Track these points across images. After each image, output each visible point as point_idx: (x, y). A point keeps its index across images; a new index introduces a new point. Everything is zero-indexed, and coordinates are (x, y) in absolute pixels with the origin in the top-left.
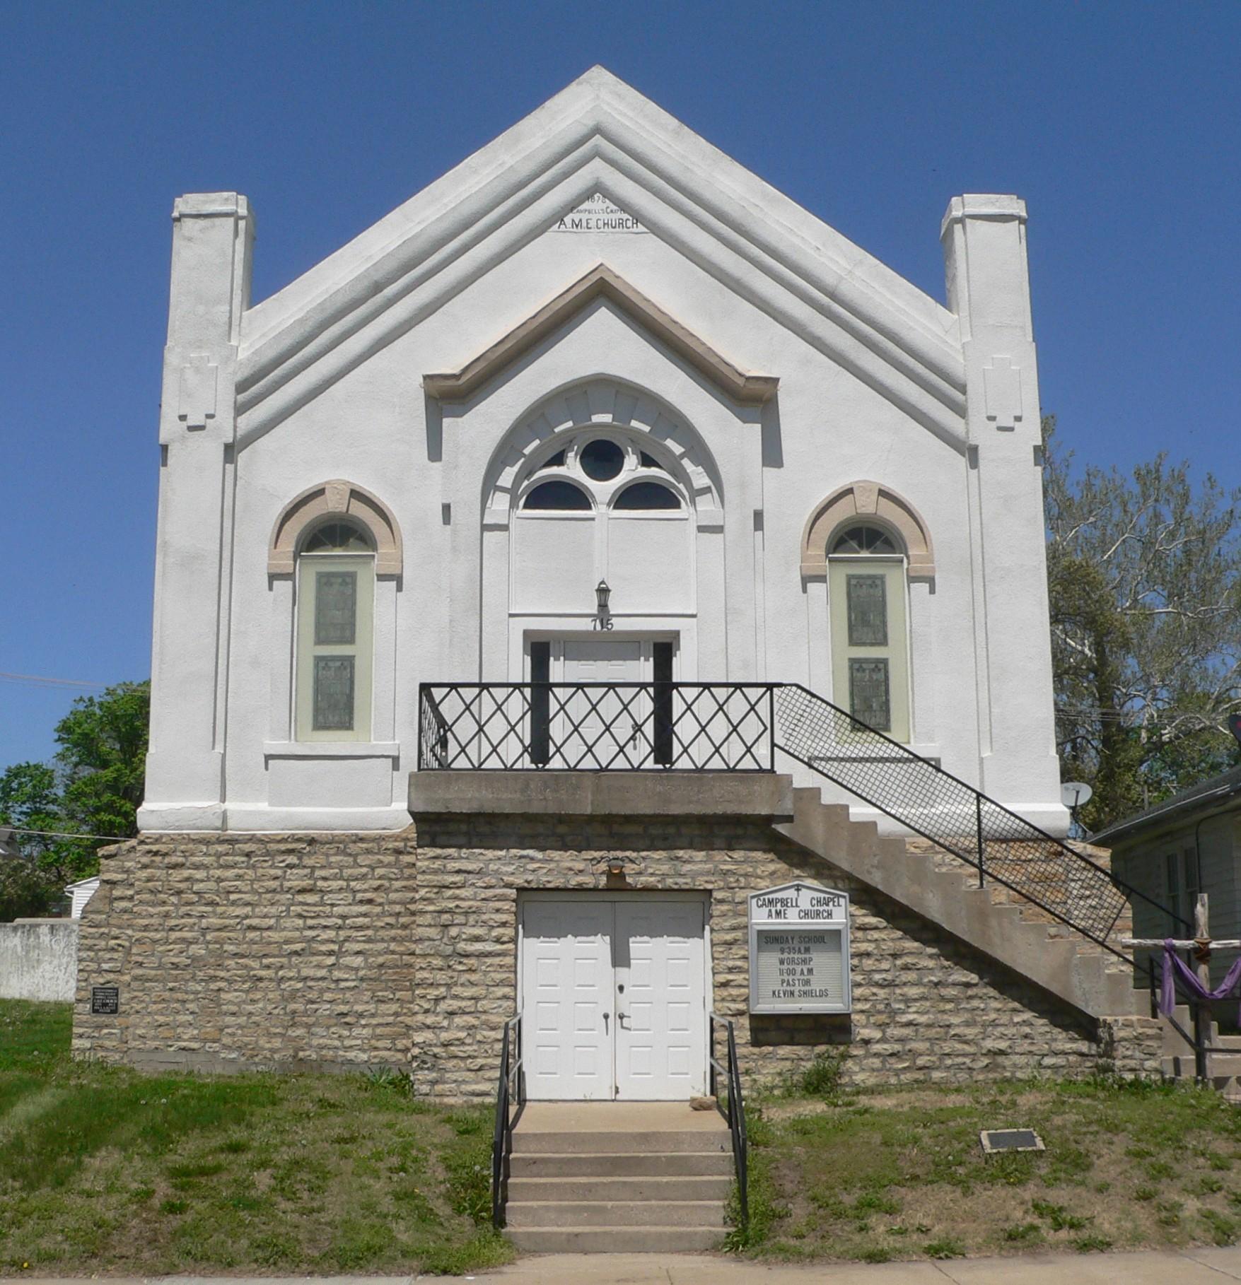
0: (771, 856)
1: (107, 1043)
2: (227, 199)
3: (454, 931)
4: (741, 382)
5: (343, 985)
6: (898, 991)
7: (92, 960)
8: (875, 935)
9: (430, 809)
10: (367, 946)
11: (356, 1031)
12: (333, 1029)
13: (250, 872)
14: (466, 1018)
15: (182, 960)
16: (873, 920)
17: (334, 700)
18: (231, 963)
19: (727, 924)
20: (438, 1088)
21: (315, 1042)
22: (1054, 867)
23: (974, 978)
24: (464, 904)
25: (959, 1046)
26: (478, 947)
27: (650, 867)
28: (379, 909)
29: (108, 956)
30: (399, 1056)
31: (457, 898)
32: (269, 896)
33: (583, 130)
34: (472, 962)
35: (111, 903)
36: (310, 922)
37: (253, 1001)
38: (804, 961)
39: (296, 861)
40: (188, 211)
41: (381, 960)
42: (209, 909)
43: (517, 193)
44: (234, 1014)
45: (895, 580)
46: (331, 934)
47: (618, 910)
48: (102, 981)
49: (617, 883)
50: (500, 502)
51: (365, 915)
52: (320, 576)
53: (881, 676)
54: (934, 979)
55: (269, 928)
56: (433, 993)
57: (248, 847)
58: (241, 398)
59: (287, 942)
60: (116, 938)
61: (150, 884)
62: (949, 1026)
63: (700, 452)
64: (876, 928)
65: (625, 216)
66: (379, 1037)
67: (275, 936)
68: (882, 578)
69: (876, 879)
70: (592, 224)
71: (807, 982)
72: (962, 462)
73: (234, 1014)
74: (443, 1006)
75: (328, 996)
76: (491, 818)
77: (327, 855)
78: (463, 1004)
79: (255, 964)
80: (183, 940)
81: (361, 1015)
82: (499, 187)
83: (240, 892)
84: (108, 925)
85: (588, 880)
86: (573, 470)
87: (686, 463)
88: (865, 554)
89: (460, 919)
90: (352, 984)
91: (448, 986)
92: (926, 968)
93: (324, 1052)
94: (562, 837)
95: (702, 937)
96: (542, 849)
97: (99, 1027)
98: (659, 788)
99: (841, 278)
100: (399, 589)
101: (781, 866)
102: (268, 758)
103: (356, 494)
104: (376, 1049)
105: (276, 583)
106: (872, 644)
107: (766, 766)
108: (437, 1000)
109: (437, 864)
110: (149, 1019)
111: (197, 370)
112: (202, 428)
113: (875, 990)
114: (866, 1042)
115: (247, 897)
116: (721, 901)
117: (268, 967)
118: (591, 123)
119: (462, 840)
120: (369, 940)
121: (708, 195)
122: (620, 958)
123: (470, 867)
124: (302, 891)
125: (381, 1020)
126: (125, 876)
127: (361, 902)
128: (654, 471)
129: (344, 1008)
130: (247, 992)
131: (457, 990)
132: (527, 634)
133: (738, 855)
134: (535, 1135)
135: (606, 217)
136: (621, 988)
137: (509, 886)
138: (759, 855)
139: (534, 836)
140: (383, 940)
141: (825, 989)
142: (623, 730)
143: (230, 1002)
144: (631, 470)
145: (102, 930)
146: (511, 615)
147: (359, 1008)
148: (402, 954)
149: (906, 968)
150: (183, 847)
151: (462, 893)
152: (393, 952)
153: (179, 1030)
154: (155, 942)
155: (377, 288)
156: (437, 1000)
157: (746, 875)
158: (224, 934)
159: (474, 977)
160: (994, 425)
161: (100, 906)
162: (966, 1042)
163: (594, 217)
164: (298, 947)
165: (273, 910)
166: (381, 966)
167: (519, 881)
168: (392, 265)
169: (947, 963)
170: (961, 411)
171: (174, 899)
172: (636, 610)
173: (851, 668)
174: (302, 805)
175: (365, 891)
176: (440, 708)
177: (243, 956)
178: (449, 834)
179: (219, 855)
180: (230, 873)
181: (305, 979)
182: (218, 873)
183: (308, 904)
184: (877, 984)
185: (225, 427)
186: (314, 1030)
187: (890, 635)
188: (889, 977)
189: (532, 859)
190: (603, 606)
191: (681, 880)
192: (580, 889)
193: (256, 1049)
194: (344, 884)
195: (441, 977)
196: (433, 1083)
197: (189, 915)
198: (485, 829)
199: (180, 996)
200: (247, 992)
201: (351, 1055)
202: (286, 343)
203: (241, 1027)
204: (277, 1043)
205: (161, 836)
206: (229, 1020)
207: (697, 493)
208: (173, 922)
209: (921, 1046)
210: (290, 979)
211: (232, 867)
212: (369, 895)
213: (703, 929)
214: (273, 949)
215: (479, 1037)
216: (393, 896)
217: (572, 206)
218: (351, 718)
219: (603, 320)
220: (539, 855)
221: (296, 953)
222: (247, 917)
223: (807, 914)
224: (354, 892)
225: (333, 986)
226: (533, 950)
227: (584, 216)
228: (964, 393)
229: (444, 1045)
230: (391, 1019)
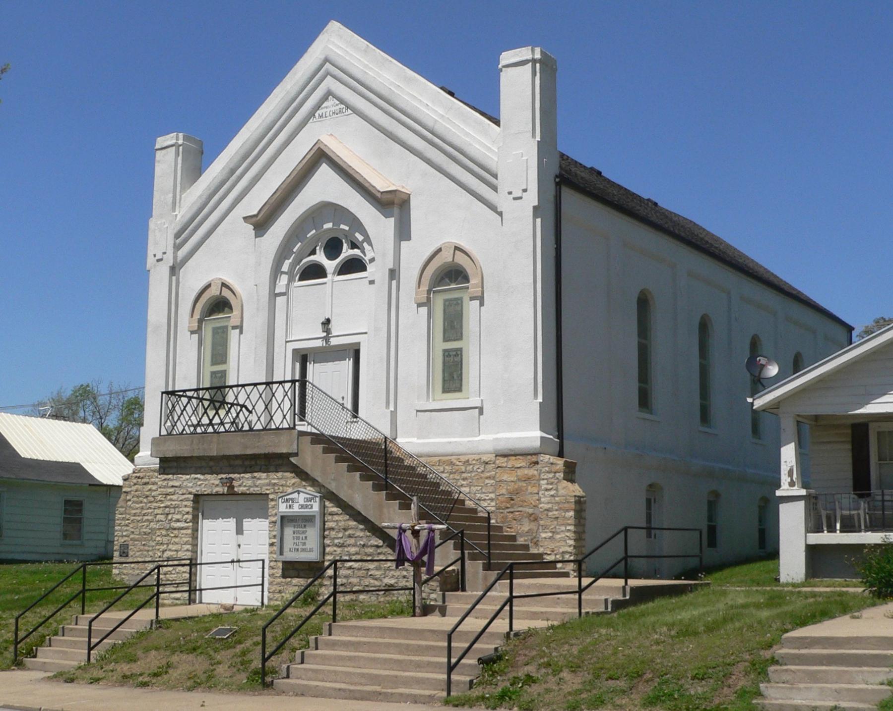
0: (293, 475)
3: (170, 517)
6: (346, 549)
8: (336, 518)
15: (148, 531)
16: (335, 509)
17: (452, 374)
22: (532, 472)
23: (380, 543)
24: (174, 503)
25: (372, 581)
27: (245, 482)
31: (171, 500)
34: (176, 532)
38: (304, 532)
43: (292, 105)
47: (241, 505)
49: (232, 493)
50: (283, 280)
52: (445, 301)
53: (457, 359)
54: (362, 543)
58: (178, 241)
62: (368, 570)
64: (337, 514)
70: (328, 114)
71: (304, 544)
76: (185, 459)
80: (148, 520)
86: (320, 257)
89: (172, 511)
92: (358, 537)
94: (211, 467)
96: (203, 474)
99: (436, 121)
100: (241, 332)
101: (297, 480)
102: (418, 411)
106: (455, 340)
109: (165, 483)
112: (521, 198)
113: (335, 548)
118: (323, 57)
121: (374, 86)
122: (239, 531)
131: (170, 547)
133: (279, 474)
134: (416, 630)
135: (333, 109)
136: (239, 546)
137: (190, 493)
138: (288, 474)
139: (201, 467)
141: (305, 547)
144: (347, 252)
146: (366, 333)
149: (350, 536)
155: (232, 172)
157: (282, 485)
160: (511, 196)
162: (376, 579)
163: (328, 110)
167: (194, 491)
168: (238, 157)
169: (368, 534)
171: (145, 500)
173: (444, 355)
184: (336, 546)
185: (169, 260)
188: (341, 541)
189: (199, 479)
191: (256, 489)
192: (217, 494)
195: (165, 540)
198: (182, 465)
199: (146, 548)
202: (195, 209)
209: (354, 580)
217: (318, 106)
220: (202, 477)
223: (302, 507)
227: (323, 111)
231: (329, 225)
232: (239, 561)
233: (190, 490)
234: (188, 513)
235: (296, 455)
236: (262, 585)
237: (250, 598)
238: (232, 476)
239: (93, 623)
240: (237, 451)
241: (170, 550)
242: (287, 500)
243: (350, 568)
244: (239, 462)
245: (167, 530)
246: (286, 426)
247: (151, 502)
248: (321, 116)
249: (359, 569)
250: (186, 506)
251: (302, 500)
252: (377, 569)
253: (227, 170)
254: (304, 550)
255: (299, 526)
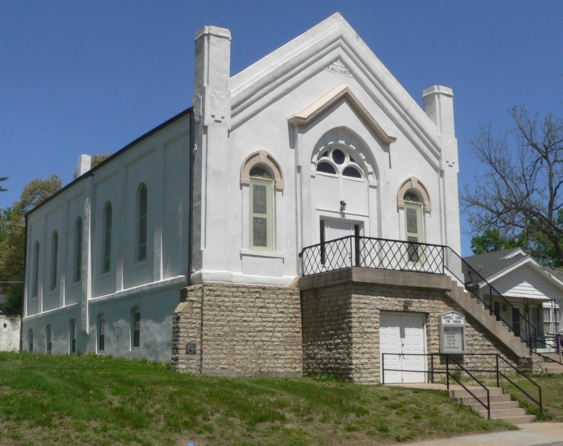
0: (443, 302)
1: (192, 366)
2: (226, 32)
3: (363, 324)
4: (386, 137)
5: (275, 343)
7: (185, 332)
9: (359, 281)
10: (282, 329)
11: (279, 361)
12: (272, 360)
13: (244, 299)
14: (367, 355)
17: (260, 235)
18: (238, 334)
19: (433, 324)
20: (361, 379)
21: (266, 365)
23: (490, 343)
24: (366, 315)
25: (488, 365)
26: (370, 330)
27: (417, 305)
28: (285, 315)
29: (191, 331)
30: (293, 370)
31: (363, 312)
32: (250, 309)
33: (337, 36)
34: (368, 335)
35: (192, 309)
36: (264, 319)
37: (246, 349)
39: (259, 296)
40: (213, 33)
41: (287, 334)
42: (230, 313)
44: (239, 354)
45: (419, 212)
46: (271, 324)
47: (403, 318)
48: (189, 341)
51: (281, 317)
55: (251, 321)
56: (358, 346)
57: (243, 290)
59: (257, 327)
60: (194, 324)
61: (209, 302)
63: (371, 159)
65: (347, 70)
66: (287, 363)
67: (253, 324)
68: (415, 210)
69: (470, 311)
70: (337, 70)
72: (436, 175)
73: (239, 354)
74: (361, 351)
75: (270, 348)
77: (269, 294)
78: (367, 350)
79: (246, 335)
81: (281, 355)
82: (313, 50)
83: (241, 307)
84: (191, 318)
85: (398, 308)
86: (330, 159)
87: (365, 162)
88: (411, 202)
89: (364, 320)
90: (278, 343)
91: (362, 344)
93: (269, 369)
95: (423, 328)
96: (386, 297)
97: (189, 360)
98: (419, 278)
101: (445, 306)
103: (269, 157)
104: (286, 367)
105: (244, 187)
107: (442, 273)
108: (359, 348)
110: (210, 356)
111: (218, 98)
112: (220, 122)
114: (467, 363)
115: (243, 309)
116: (432, 317)
117: (250, 336)
118: (340, 34)
119: (364, 292)
120: (283, 327)
121: (373, 69)
122: (403, 335)
123: (367, 302)
124: (262, 307)
125: (287, 357)
126: (197, 299)
127: (280, 312)
128: (353, 163)
129: (275, 352)
130: (243, 346)
131: (365, 345)
132: (321, 217)
133: (436, 301)
136: (403, 345)
137: (378, 309)
138: (440, 302)
139: (383, 292)
140: (287, 327)
141: (453, 345)
142: (398, 256)
143: (238, 350)
145: (189, 320)
147: (280, 352)
148: (293, 332)
149: (475, 340)
150: (221, 288)
151: (365, 311)
152: (290, 332)
153: (221, 361)
154: (211, 325)
155: (275, 79)
156: (359, 348)
157: (438, 308)
158: (235, 323)
159: (369, 341)
161: (188, 310)
163: (338, 68)
164: (260, 329)
165: (251, 314)
166: (287, 336)
167: (381, 307)
168: (280, 71)
170: (438, 158)
171: (218, 309)
172: (354, 212)
173: (254, 221)
174: (255, 274)
175: (281, 308)
176: (319, 242)
177: (242, 332)
178: (360, 290)
179: (233, 292)
180: (237, 299)
181: (263, 341)
182: (233, 299)
183: (263, 312)
185: (230, 122)
186: (266, 360)
187: (418, 230)
190: (342, 209)
191: (422, 309)
192: (396, 311)
193: (247, 368)
194: (274, 305)
196: (359, 378)
197: (223, 315)
198: (370, 289)
199: (221, 347)
200: (243, 346)
201: (278, 370)
202: (247, 94)
203: (242, 359)
204: (254, 365)
205: (213, 283)
206: (238, 357)
207: (367, 174)
208: (218, 318)
209: (479, 365)
210: (258, 341)
211: (238, 297)
212: (283, 310)
213: (423, 326)
214: (252, 329)
215: (371, 362)
216: (290, 311)
217: (331, 63)
218: (266, 242)
219: (345, 107)
221: (260, 331)
222: (243, 317)
223: (455, 322)
224: (278, 308)
225: (271, 344)
226: (382, 330)
227: (335, 67)
228: (440, 152)
229: (362, 364)
230: (290, 356)
231: (342, 142)
232: (403, 354)
233: (378, 306)
234: (377, 322)
235: (450, 291)
236: (383, 370)
237: (419, 380)
238: (412, 300)
239: (486, 392)
240: (416, 284)
241: (364, 347)
242: (446, 317)
243: (477, 358)
244: (409, 291)
245: (361, 333)
246: (437, 272)
247: (223, 311)
248: (333, 69)
249: (481, 358)
250: (375, 317)
251: (454, 319)
252: (489, 358)
253: (271, 77)
254: (454, 348)
255: (450, 333)
